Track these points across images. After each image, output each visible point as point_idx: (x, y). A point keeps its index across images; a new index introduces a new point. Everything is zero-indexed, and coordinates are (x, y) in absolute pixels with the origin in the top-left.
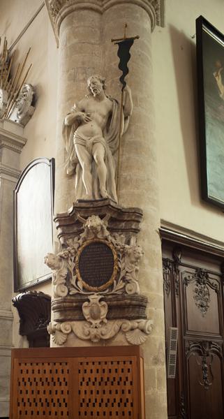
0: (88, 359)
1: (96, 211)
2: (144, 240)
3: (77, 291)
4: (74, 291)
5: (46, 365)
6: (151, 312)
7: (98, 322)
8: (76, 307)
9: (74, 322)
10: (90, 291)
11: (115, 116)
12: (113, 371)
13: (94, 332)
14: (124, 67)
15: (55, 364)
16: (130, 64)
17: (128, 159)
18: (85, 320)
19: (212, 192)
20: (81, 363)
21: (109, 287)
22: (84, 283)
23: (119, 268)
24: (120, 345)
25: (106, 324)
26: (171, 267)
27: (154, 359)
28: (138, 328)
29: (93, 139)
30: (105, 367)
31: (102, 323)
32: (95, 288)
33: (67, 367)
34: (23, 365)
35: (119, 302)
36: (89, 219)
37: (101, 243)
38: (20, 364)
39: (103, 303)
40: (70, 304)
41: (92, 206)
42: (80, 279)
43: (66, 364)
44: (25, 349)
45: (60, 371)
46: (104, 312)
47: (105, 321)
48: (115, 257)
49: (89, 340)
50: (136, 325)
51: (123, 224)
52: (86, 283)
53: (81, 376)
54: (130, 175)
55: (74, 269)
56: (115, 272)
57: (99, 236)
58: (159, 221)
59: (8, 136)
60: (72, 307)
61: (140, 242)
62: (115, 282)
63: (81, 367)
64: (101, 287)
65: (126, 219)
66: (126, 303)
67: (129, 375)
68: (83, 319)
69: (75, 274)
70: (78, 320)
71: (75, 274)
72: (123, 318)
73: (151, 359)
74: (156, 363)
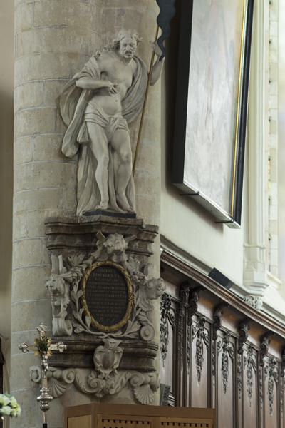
0: (169, 420)
1: (121, 228)
3: (83, 329)
4: (80, 329)
7: (108, 372)
9: (78, 370)
10: (99, 331)
19: (189, 181)
20: (162, 423)
24: (125, 403)
28: (149, 383)
31: (112, 373)
34: (106, 422)
35: (137, 350)
36: (113, 236)
37: (114, 268)
38: (103, 421)
41: (118, 222)
43: (148, 423)
44: (157, 406)
46: (117, 361)
50: (149, 379)
52: (96, 320)
55: (80, 299)
57: (114, 259)
58: (262, 304)
64: (114, 327)
65: (142, 238)
66: (145, 352)
68: (91, 366)
71: (81, 306)
72: (132, 369)
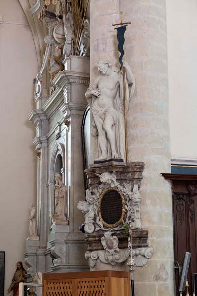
2: (147, 185)
4: (98, 229)
5: (61, 283)
6: (152, 241)
7: (113, 250)
8: (98, 240)
9: (99, 251)
10: (107, 228)
11: (121, 87)
12: (96, 286)
13: (111, 258)
14: (120, 48)
15: (65, 283)
16: (125, 47)
17: (135, 119)
18: (104, 249)
21: (120, 225)
22: (104, 222)
23: (126, 210)
25: (119, 252)
26: (184, 198)
27: (154, 277)
28: (140, 254)
29: (105, 109)
30: (91, 284)
31: (115, 251)
32: (111, 226)
33: (71, 285)
39: (115, 237)
40: (94, 239)
42: (101, 219)
45: (68, 287)
47: (118, 249)
48: (123, 201)
49: (109, 264)
51: (130, 174)
53: (79, 290)
54: (136, 133)
56: (123, 214)
59: (57, 94)
60: (95, 240)
61: (143, 188)
62: (123, 220)
63: (79, 285)
64: (114, 225)
65: (130, 171)
67: (104, 289)
68: (103, 249)
69: (98, 215)
70: (100, 250)
73: (152, 276)
74: (157, 280)
